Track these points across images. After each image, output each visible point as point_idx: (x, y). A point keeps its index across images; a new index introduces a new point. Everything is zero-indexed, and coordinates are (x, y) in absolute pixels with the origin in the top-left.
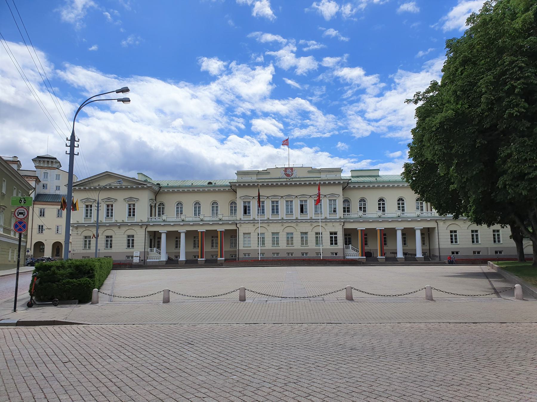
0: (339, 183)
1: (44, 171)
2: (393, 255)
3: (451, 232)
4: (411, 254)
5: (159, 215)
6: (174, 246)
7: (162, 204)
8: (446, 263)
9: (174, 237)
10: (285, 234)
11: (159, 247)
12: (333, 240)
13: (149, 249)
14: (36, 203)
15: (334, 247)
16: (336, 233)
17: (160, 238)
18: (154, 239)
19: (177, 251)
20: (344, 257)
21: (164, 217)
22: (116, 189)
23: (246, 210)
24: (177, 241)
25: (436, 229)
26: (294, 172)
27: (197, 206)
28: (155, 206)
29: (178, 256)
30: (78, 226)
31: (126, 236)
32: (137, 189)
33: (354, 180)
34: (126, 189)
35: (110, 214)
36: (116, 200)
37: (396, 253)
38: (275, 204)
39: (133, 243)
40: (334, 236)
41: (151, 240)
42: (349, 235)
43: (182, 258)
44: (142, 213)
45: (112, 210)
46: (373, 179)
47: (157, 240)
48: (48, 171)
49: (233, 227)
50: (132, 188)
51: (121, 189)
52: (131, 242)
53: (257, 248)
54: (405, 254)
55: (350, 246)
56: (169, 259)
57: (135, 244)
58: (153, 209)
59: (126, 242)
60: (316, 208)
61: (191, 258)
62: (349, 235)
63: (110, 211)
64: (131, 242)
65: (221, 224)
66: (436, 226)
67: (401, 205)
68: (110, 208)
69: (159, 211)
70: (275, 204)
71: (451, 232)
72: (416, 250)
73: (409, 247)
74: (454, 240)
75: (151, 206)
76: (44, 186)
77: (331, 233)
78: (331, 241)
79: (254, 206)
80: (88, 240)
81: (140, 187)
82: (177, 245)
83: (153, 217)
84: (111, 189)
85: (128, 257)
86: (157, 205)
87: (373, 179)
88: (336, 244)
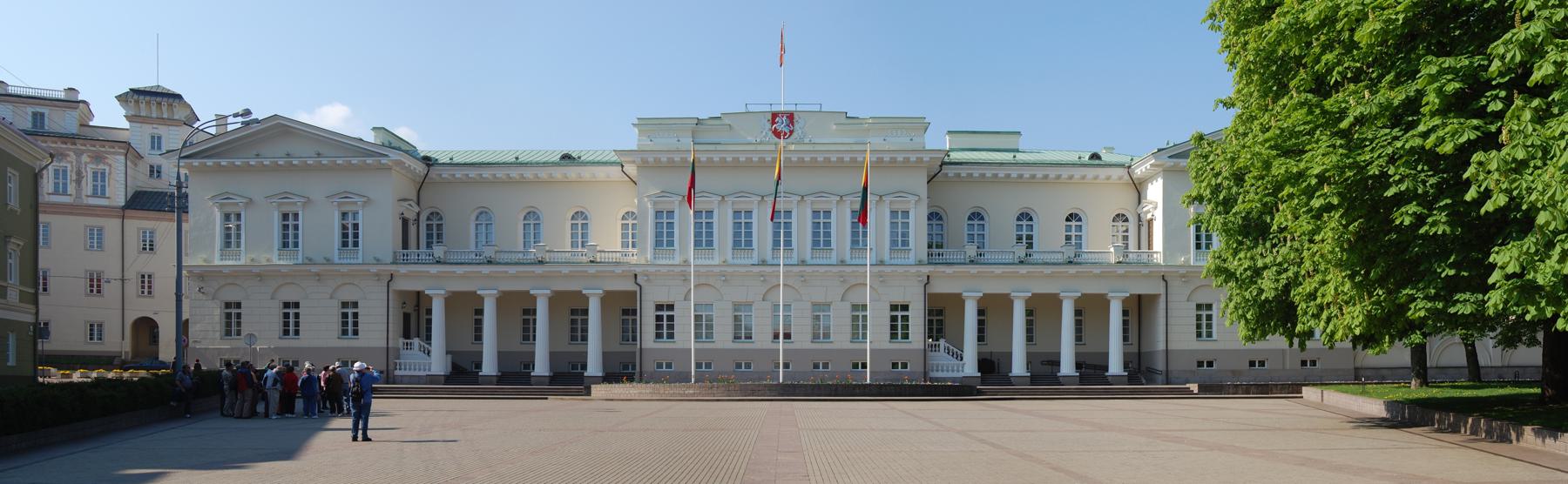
0: (920, 160)
1: (148, 130)
2: (1048, 369)
3: (1199, 307)
4: (1095, 367)
5: (429, 245)
6: (519, 333)
7: (435, 215)
8: (683, 378)
9: (466, 307)
10: (849, 306)
11: (429, 338)
12: (898, 327)
13: (402, 341)
14: (129, 212)
15: (899, 345)
16: (905, 308)
17: (429, 312)
18: (413, 318)
19: (525, 348)
20: (925, 373)
21: (438, 251)
22: (306, 168)
23: (742, 239)
24: (526, 322)
25: (1163, 299)
26: (797, 126)
27: (580, 222)
28: (417, 220)
29: (530, 364)
30: (204, 275)
31: (336, 304)
32: (365, 168)
33: (955, 156)
34: (334, 168)
35: (291, 240)
36: (250, 202)
37: (1058, 364)
38: (900, 220)
39: (356, 324)
40: (899, 314)
41: (406, 317)
42: (940, 312)
43: (541, 368)
44: (379, 232)
45: (296, 227)
46: (1008, 157)
47: (424, 317)
48: (161, 130)
49: (629, 286)
50: (349, 168)
51: (320, 168)
52: (349, 322)
53: (774, 346)
54: (1078, 366)
55: (942, 342)
56: (455, 366)
57: (360, 328)
58: (412, 229)
59: (338, 319)
60: (855, 234)
61: (565, 368)
62: (940, 312)
63: (291, 231)
64: (349, 322)
65: (1023, 276)
66: (1162, 291)
67: (1073, 233)
68: (291, 222)
69: (429, 236)
70: (900, 220)
71: (1199, 307)
72: (1059, 354)
73: (993, 347)
74: (1204, 330)
75: (405, 222)
76: (152, 172)
77: (894, 308)
78: (894, 327)
79: (762, 228)
80: (350, 311)
81: (369, 161)
82: (528, 333)
83: (412, 249)
84: (290, 168)
85: (574, 367)
86: (423, 217)
87: (1008, 157)
88: (906, 336)
